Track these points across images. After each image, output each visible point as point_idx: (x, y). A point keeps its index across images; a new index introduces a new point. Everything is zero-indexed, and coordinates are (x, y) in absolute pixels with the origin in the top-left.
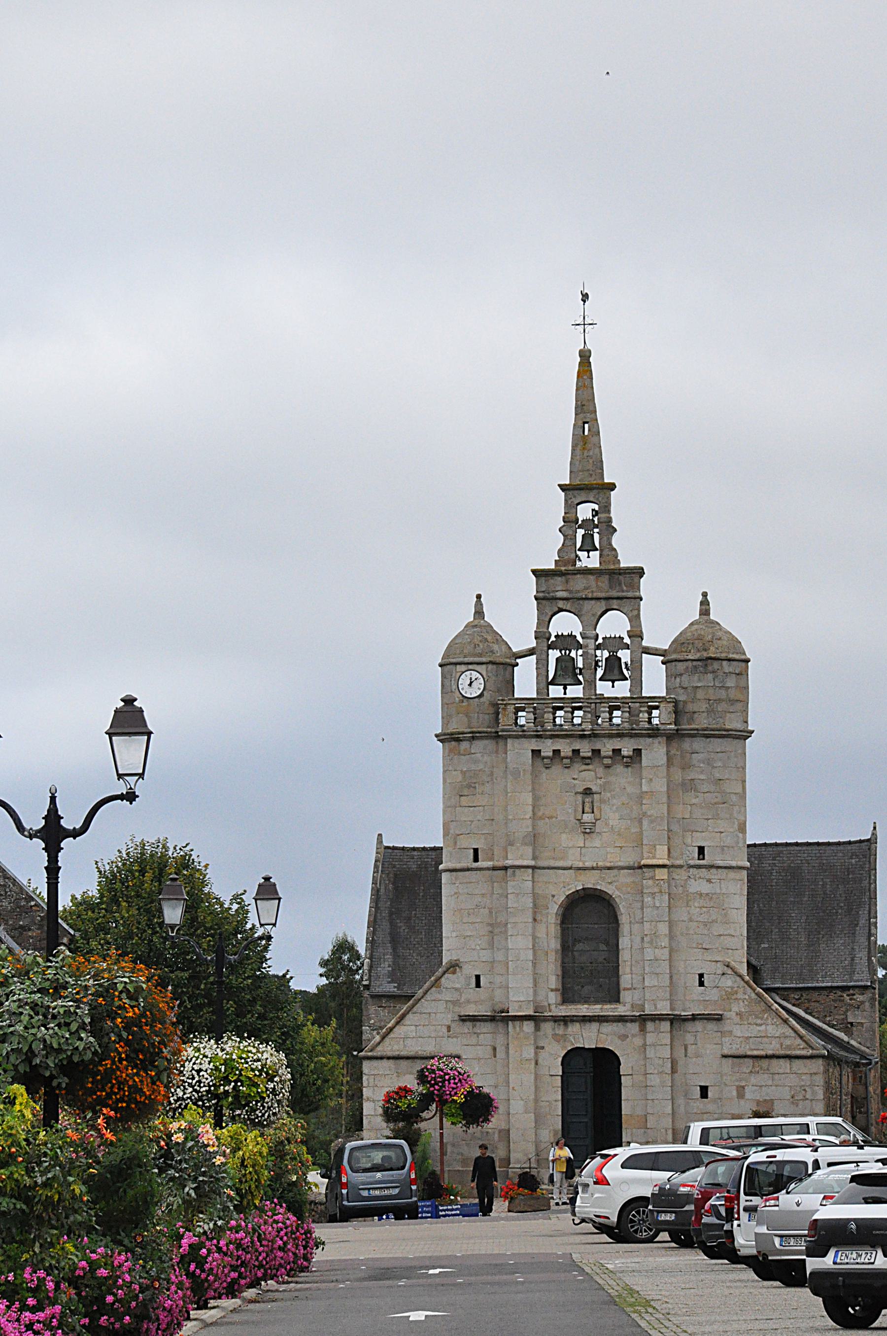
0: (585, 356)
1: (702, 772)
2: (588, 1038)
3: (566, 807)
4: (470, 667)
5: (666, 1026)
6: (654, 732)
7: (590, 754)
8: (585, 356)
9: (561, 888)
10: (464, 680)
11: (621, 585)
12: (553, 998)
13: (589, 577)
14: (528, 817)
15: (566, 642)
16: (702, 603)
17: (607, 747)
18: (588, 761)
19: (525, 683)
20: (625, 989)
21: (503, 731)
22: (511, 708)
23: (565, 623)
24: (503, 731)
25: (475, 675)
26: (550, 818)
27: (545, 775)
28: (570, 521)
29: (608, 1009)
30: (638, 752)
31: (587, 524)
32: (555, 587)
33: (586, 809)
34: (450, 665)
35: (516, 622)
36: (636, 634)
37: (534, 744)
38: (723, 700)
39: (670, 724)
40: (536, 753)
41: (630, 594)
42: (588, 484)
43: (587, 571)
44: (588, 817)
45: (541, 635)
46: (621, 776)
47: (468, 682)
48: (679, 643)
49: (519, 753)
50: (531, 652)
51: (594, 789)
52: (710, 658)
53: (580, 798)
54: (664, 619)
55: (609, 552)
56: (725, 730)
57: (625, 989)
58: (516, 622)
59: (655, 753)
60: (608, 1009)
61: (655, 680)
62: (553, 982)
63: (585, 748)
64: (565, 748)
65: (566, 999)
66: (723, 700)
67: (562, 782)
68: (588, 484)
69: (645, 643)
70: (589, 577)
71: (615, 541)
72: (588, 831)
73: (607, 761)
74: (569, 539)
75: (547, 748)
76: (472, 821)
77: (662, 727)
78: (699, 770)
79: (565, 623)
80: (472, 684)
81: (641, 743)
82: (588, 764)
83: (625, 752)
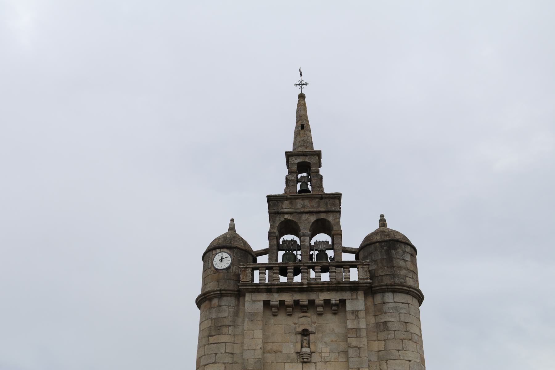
0: (302, 97)
1: (391, 316)
3: (291, 346)
4: (222, 250)
6: (354, 287)
7: (306, 303)
8: (302, 97)
10: (217, 258)
11: (325, 211)
14: (259, 347)
16: (380, 220)
17: (321, 297)
18: (305, 309)
21: (242, 286)
22: (250, 270)
24: (242, 286)
25: (225, 255)
26: (276, 352)
27: (273, 320)
30: (343, 302)
33: (304, 344)
34: (208, 255)
35: (256, 233)
37: (264, 297)
39: (367, 279)
40: (267, 304)
41: (333, 209)
42: (302, 126)
44: (306, 350)
46: (331, 323)
47: (220, 258)
49: (253, 304)
51: (310, 329)
52: (389, 252)
53: (299, 337)
54: (355, 230)
56: (407, 287)
58: (256, 233)
59: (357, 303)
63: (303, 299)
64: (288, 298)
67: (284, 327)
68: (302, 126)
69: (344, 245)
72: (305, 360)
73: (320, 309)
75: (275, 299)
76: (216, 354)
77: (361, 281)
78: (389, 314)
80: (223, 260)
81: (346, 295)
82: (306, 312)
83: (333, 301)
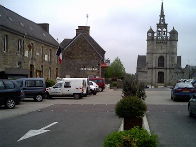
0: (162, 3)
2: (161, 70)
5: (169, 70)
8: (162, 3)
9: (158, 55)
11: (165, 26)
12: (157, 66)
13: (162, 25)
15: (160, 31)
17: (164, 42)
19: (155, 35)
20: (87, 25)
23: (160, 29)
28: (160, 19)
29: (163, 68)
30: (167, 42)
31: (162, 20)
32: (159, 26)
34: (148, 33)
35: (155, 29)
36: (167, 30)
38: (154, 68)
40: (157, 42)
42: (162, 15)
43: (162, 24)
45: (157, 30)
48: (171, 32)
50: (156, 32)
54: (170, 29)
55: (164, 22)
57: (87, 25)
58: (155, 29)
60: (163, 68)
61: (168, 35)
62: (157, 65)
64: (159, 41)
65: (159, 66)
66: (154, 68)
68: (162, 15)
70: (162, 25)
71: (165, 21)
74: (160, 21)
79: (160, 29)
